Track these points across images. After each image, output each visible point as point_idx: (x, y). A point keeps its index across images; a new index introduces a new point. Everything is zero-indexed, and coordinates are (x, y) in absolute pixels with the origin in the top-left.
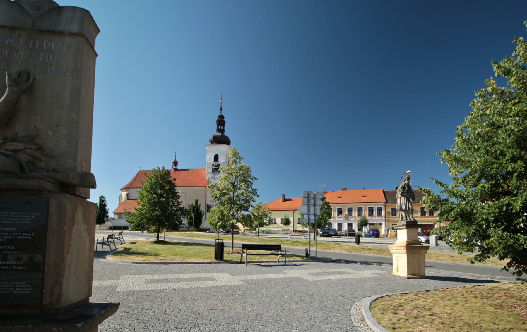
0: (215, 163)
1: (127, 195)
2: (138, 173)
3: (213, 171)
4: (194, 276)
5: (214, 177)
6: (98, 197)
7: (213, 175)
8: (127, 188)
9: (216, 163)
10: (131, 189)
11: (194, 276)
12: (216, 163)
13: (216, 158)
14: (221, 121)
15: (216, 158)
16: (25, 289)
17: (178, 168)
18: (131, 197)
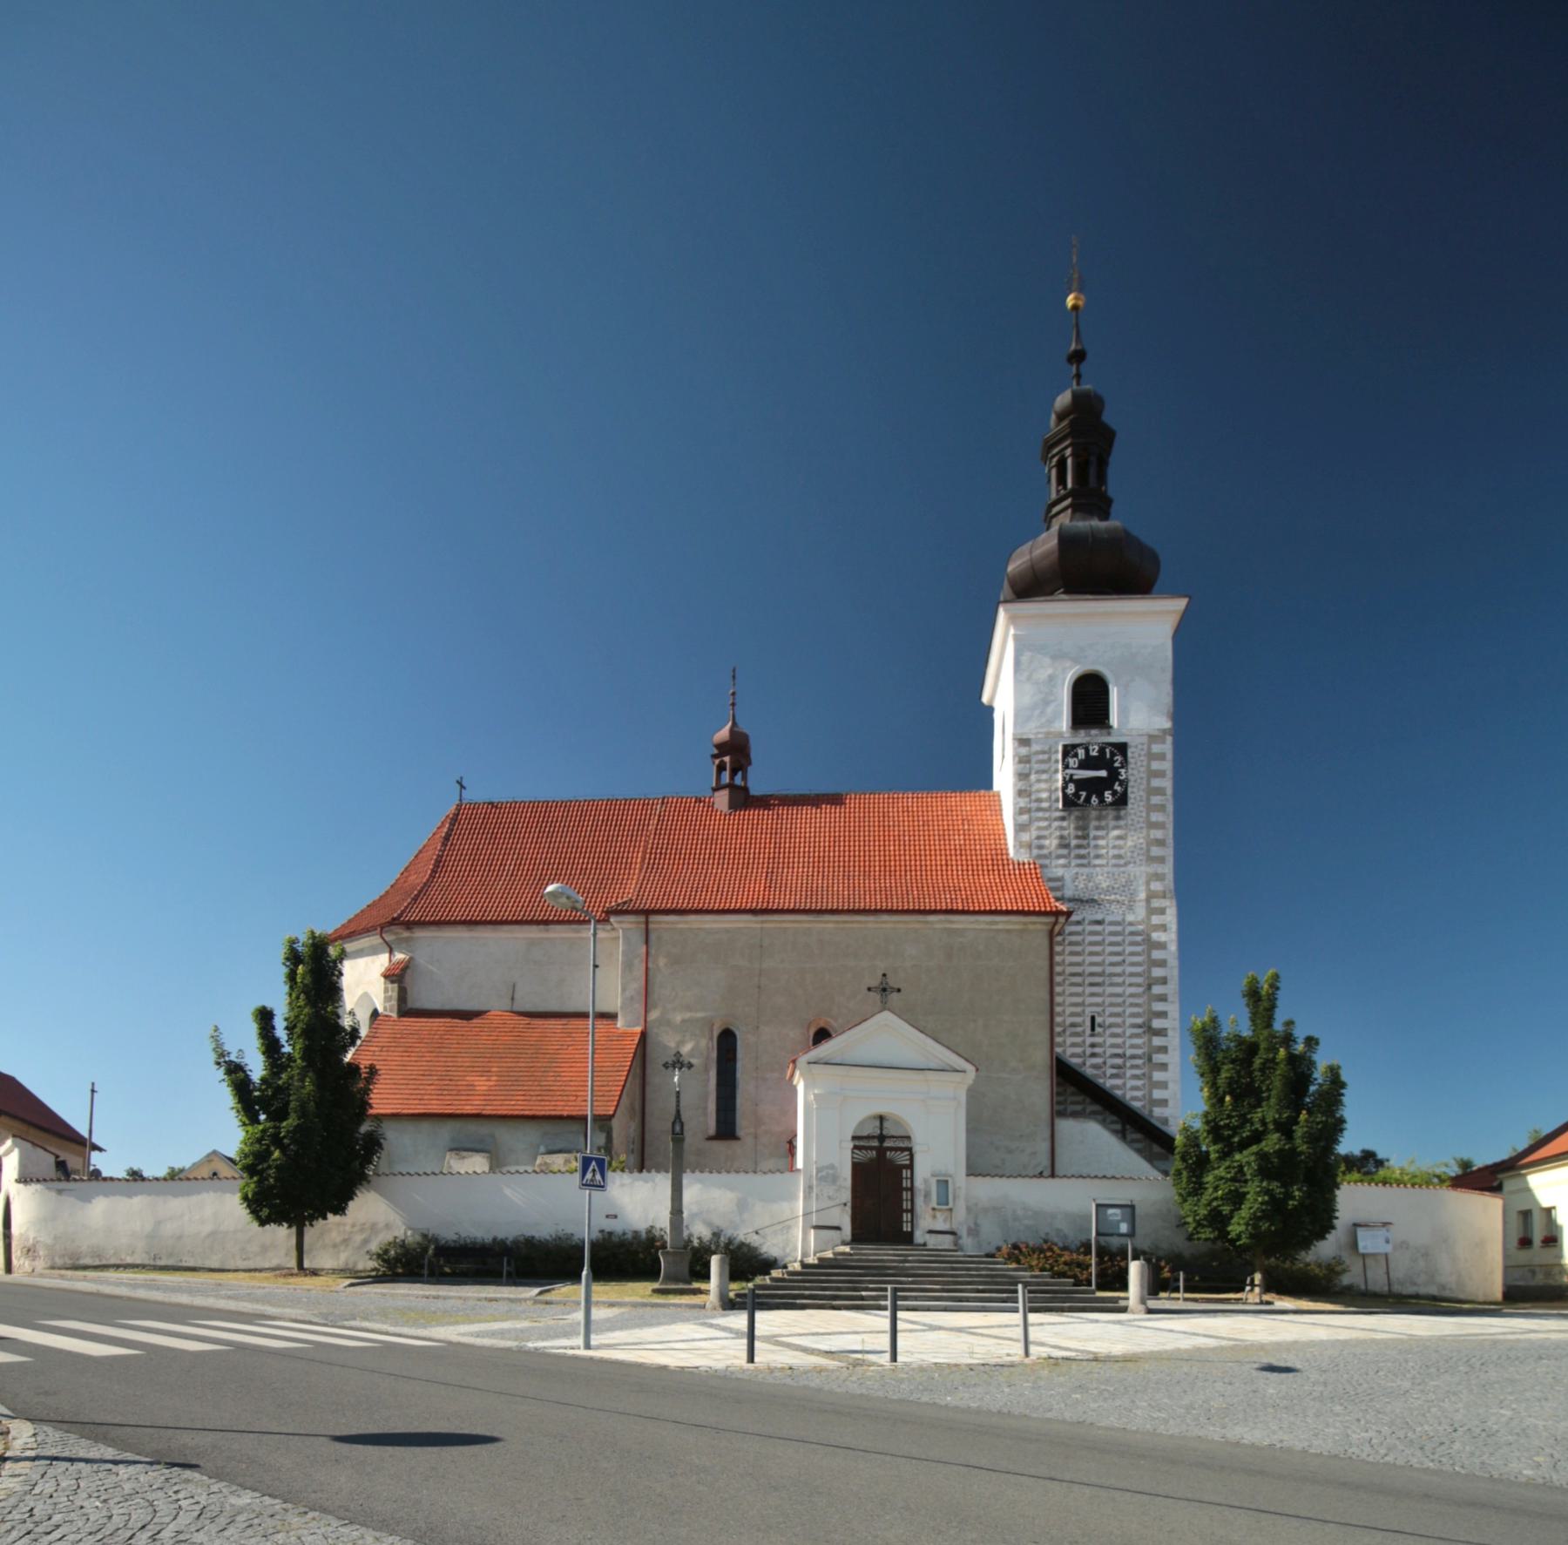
0: (1082, 737)
1: (396, 976)
2: (454, 819)
3: (1069, 803)
4: (1532, 1336)
5: (1078, 847)
6: (281, 952)
7: (1070, 828)
8: (394, 922)
9: (1094, 739)
10: (419, 933)
11: (1532, 1336)
12: (1094, 739)
13: (1090, 699)
14: (1088, 437)
15: (1090, 699)
16: (1119, 980)
17: (757, 788)
18: (424, 997)
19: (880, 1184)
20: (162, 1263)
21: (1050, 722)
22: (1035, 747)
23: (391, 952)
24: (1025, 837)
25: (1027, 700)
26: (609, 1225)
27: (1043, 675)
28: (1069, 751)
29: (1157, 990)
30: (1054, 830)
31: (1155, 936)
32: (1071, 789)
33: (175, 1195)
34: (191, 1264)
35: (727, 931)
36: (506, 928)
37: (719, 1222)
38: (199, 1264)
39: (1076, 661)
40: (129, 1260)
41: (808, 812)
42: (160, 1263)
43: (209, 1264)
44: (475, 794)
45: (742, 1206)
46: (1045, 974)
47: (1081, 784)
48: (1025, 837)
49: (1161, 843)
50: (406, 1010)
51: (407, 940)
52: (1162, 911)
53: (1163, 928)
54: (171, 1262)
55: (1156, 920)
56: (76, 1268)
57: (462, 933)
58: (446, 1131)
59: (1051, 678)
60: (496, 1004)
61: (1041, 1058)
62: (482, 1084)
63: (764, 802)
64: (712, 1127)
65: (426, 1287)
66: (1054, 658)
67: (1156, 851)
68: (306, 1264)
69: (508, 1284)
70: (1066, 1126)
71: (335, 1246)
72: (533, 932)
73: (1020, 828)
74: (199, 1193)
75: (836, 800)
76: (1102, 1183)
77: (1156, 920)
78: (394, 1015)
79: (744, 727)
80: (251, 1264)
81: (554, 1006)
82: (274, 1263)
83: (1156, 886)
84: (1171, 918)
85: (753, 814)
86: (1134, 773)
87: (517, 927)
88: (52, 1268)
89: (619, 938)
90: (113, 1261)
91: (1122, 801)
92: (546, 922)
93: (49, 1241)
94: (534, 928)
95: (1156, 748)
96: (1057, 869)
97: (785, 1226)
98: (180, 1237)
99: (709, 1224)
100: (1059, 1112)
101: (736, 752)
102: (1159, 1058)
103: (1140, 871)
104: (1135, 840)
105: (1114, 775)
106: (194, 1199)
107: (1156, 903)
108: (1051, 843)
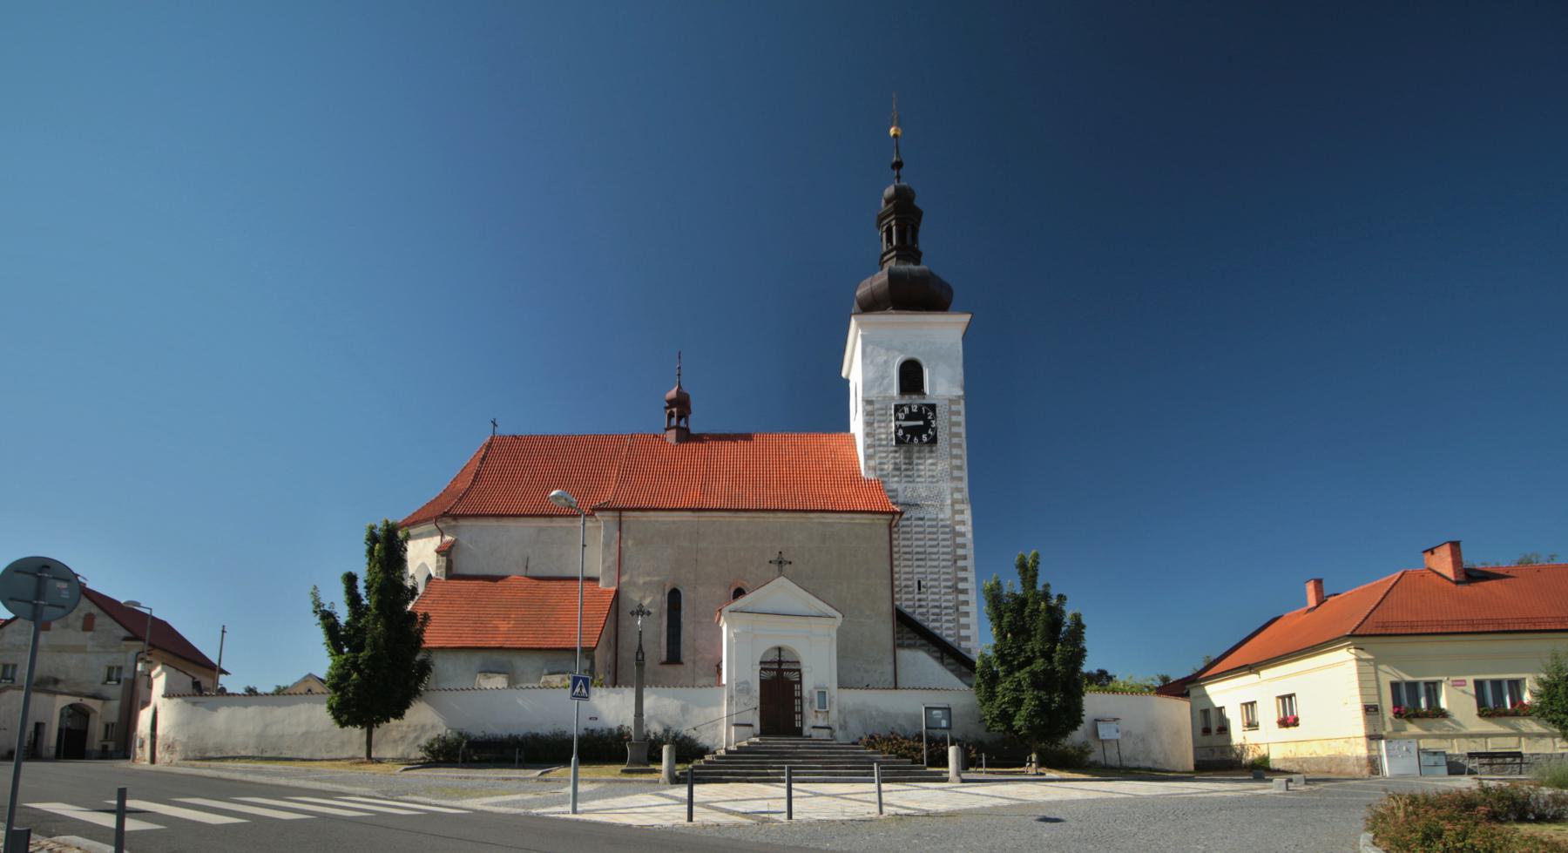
0: (906, 400)
2: (489, 446)
3: (899, 441)
5: (905, 469)
7: (900, 458)
9: (915, 401)
12: (915, 401)
13: (911, 376)
14: (905, 212)
15: (911, 376)
18: (463, 567)
19: (779, 691)
21: (886, 390)
22: (877, 406)
24: (872, 463)
25: (871, 376)
26: (592, 725)
27: (881, 359)
28: (898, 408)
31: (958, 528)
32: (901, 433)
39: (901, 351)
40: (243, 753)
41: (728, 445)
44: (505, 430)
46: (887, 552)
47: (907, 430)
48: (872, 463)
49: (959, 468)
50: (451, 574)
52: (962, 512)
53: (963, 523)
54: (273, 754)
55: (958, 518)
57: (493, 523)
58: (478, 659)
60: (515, 572)
61: (886, 608)
63: (699, 438)
67: (956, 473)
70: (904, 654)
72: (542, 522)
75: (747, 437)
76: (927, 694)
77: (958, 518)
79: (685, 389)
80: (333, 756)
81: (555, 573)
83: (957, 496)
85: (692, 445)
86: (941, 423)
89: (599, 530)
91: (933, 441)
92: (551, 516)
96: (893, 483)
97: (714, 723)
99: (661, 723)
100: (898, 645)
101: (681, 405)
102: (963, 608)
103: (946, 486)
104: (942, 466)
105: (928, 424)
106: (293, 709)
107: (958, 507)
108: (889, 467)
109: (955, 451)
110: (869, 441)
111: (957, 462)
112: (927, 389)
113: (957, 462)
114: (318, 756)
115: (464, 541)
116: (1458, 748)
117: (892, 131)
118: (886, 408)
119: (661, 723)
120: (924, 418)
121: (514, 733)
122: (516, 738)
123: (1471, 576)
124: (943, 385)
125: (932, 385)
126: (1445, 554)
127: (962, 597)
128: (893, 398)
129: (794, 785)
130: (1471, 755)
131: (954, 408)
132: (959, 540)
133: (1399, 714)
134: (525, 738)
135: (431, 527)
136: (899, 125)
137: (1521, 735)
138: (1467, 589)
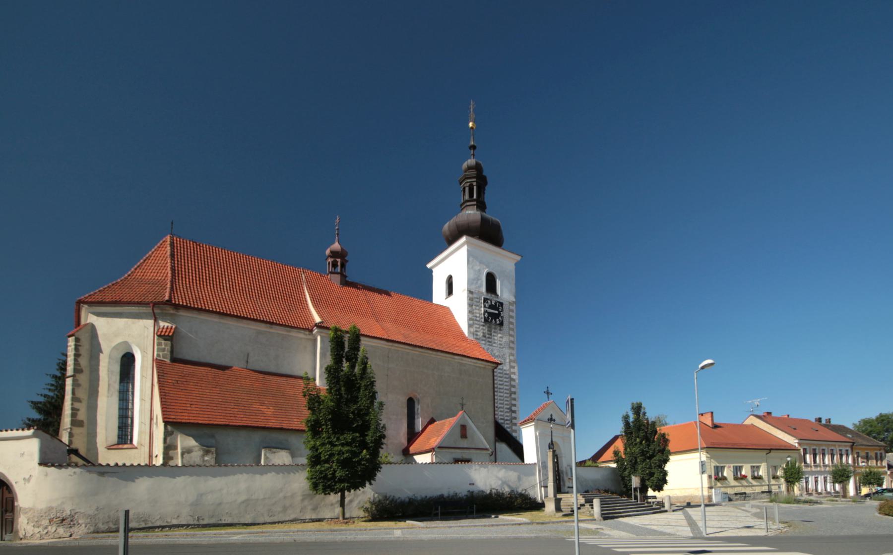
0: (489, 296)
3: (486, 320)
5: (488, 337)
7: (486, 329)
10: (182, 313)
20: (205, 522)
21: (479, 287)
22: (475, 296)
23: (156, 320)
24: (472, 330)
25: (472, 276)
26: (471, 488)
27: (477, 268)
28: (486, 300)
29: (513, 396)
30: (482, 330)
31: (512, 376)
32: (486, 315)
33: (214, 476)
34: (229, 520)
35: (372, 346)
36: (245, 321)
37: (514, 486)
38: (236, 521)
39: (487, 267)
40: (175, 522)
42: (202, 522)
43: (243, 521)
45: (519, 478)
46: (491, 386)
47: (490, 314)
48: (472, 330)
49: (513, 342)
50: (174, 360)
51: (172, 315)
52: (514, 367)
53: (514, 373)
54: (212, 521)
55: (512, 370)
56: (98, 532)
57: (216, 319)
58: (257, 436)
59: (479, 270)
60: (237, 365)
61: (490, 418)
62: (269, 411)
64: (113, 437)
65: (477, 520)
66: (481, 262)
67: (512, 345)
68: (347, 515)
69: (442, 519)
70: (497, 444)
71: (332, 505)
72: (262, 327)
73: (470, 326)
74: (234, 474)
75: (388, 294)
77: (512, 370)
78: (168, 361)
80: (276, 519)
81: (273, 369)
82: (292, 517)
83: (512, 358)
84: (516, 370)
87: (253, 323)
88: (97, 532)
90: (158, 524)
91: (501, 324)
92: (272, 323)
93: (91, 512)
94: (263, 325)
95: (511, 307)
97: (534, 486)
98: (220, 504)
99: (509, 486)
100: (496, 441)
102: (514, 421)
103: (507, 351)
104: (506, 339)
105: (499, 314)
106: (231, 478)
107: (512, 364)
108: (480, 334)
109: (511, 332)
110: (471, 316)
111: (512, 339)
112: (499, 292)
113: (512, 339)
114: (261, 520)
115: (184, 330)
116: (730, 491)
117: (471, 124)
118: (479, 298)
119: (509, 486)
120: (497, 309)
121: (458, 491)
122: (442, 496)
123: (716, 426)
124: (505, 292)
125: (502, 291)
126: (709, 416)
127: (514, 415)
128: (480, 293)
129: (130, 534)
130: (736, 494)
131: (511, 307)
132: (513, 383)
133: (716, 479)
134: (422, 500)
135: (149, 310)
136: (474, 122)
137: (743, 486)
138: (716, 430)
